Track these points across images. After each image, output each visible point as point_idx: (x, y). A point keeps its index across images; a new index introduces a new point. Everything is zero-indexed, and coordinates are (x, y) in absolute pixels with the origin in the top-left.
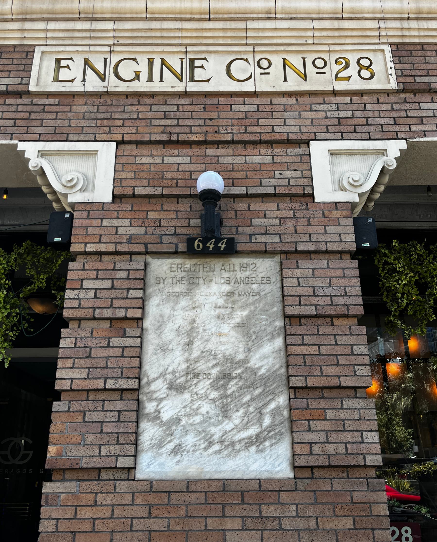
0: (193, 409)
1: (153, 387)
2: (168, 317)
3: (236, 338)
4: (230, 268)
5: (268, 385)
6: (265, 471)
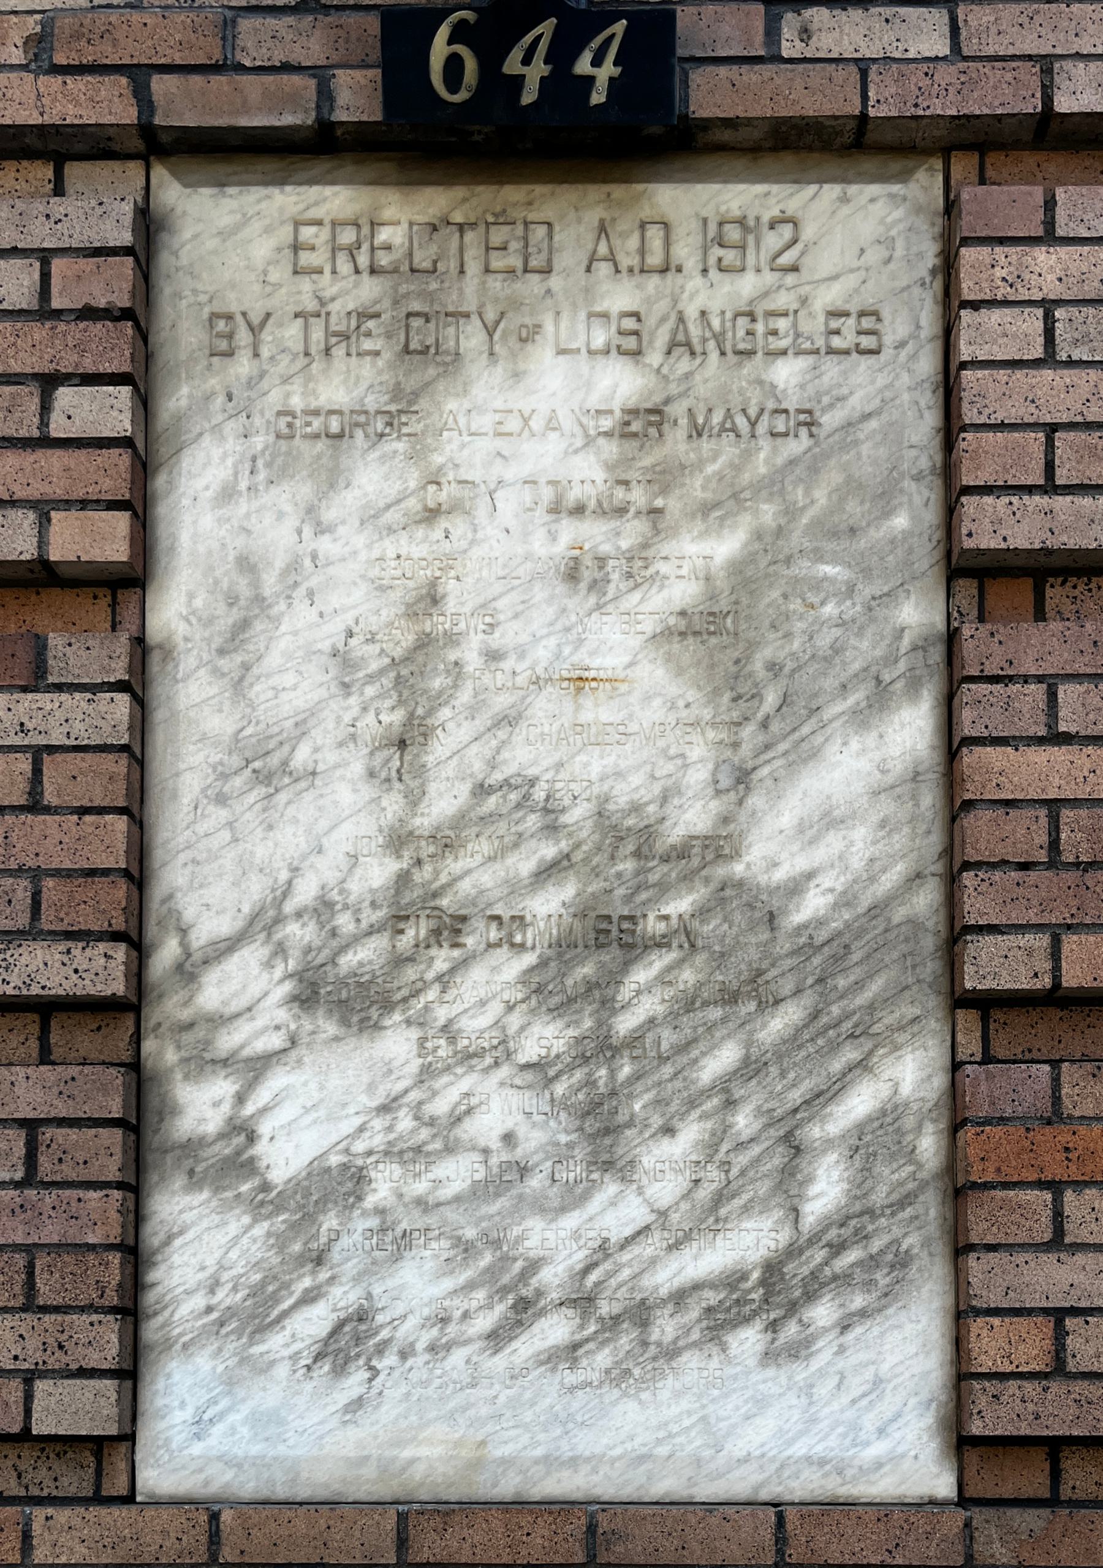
0: (432, 1122)
1: (214, 992)
2: (286, 571)
3: (673, 707)
4: (642, 251)
5: (842, 982)
6: (808, 1460)
